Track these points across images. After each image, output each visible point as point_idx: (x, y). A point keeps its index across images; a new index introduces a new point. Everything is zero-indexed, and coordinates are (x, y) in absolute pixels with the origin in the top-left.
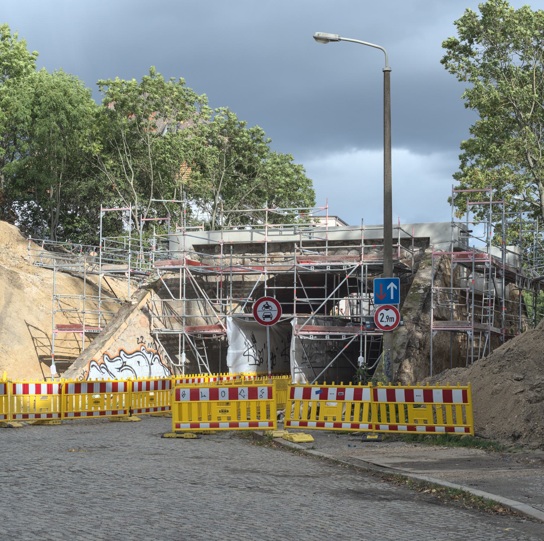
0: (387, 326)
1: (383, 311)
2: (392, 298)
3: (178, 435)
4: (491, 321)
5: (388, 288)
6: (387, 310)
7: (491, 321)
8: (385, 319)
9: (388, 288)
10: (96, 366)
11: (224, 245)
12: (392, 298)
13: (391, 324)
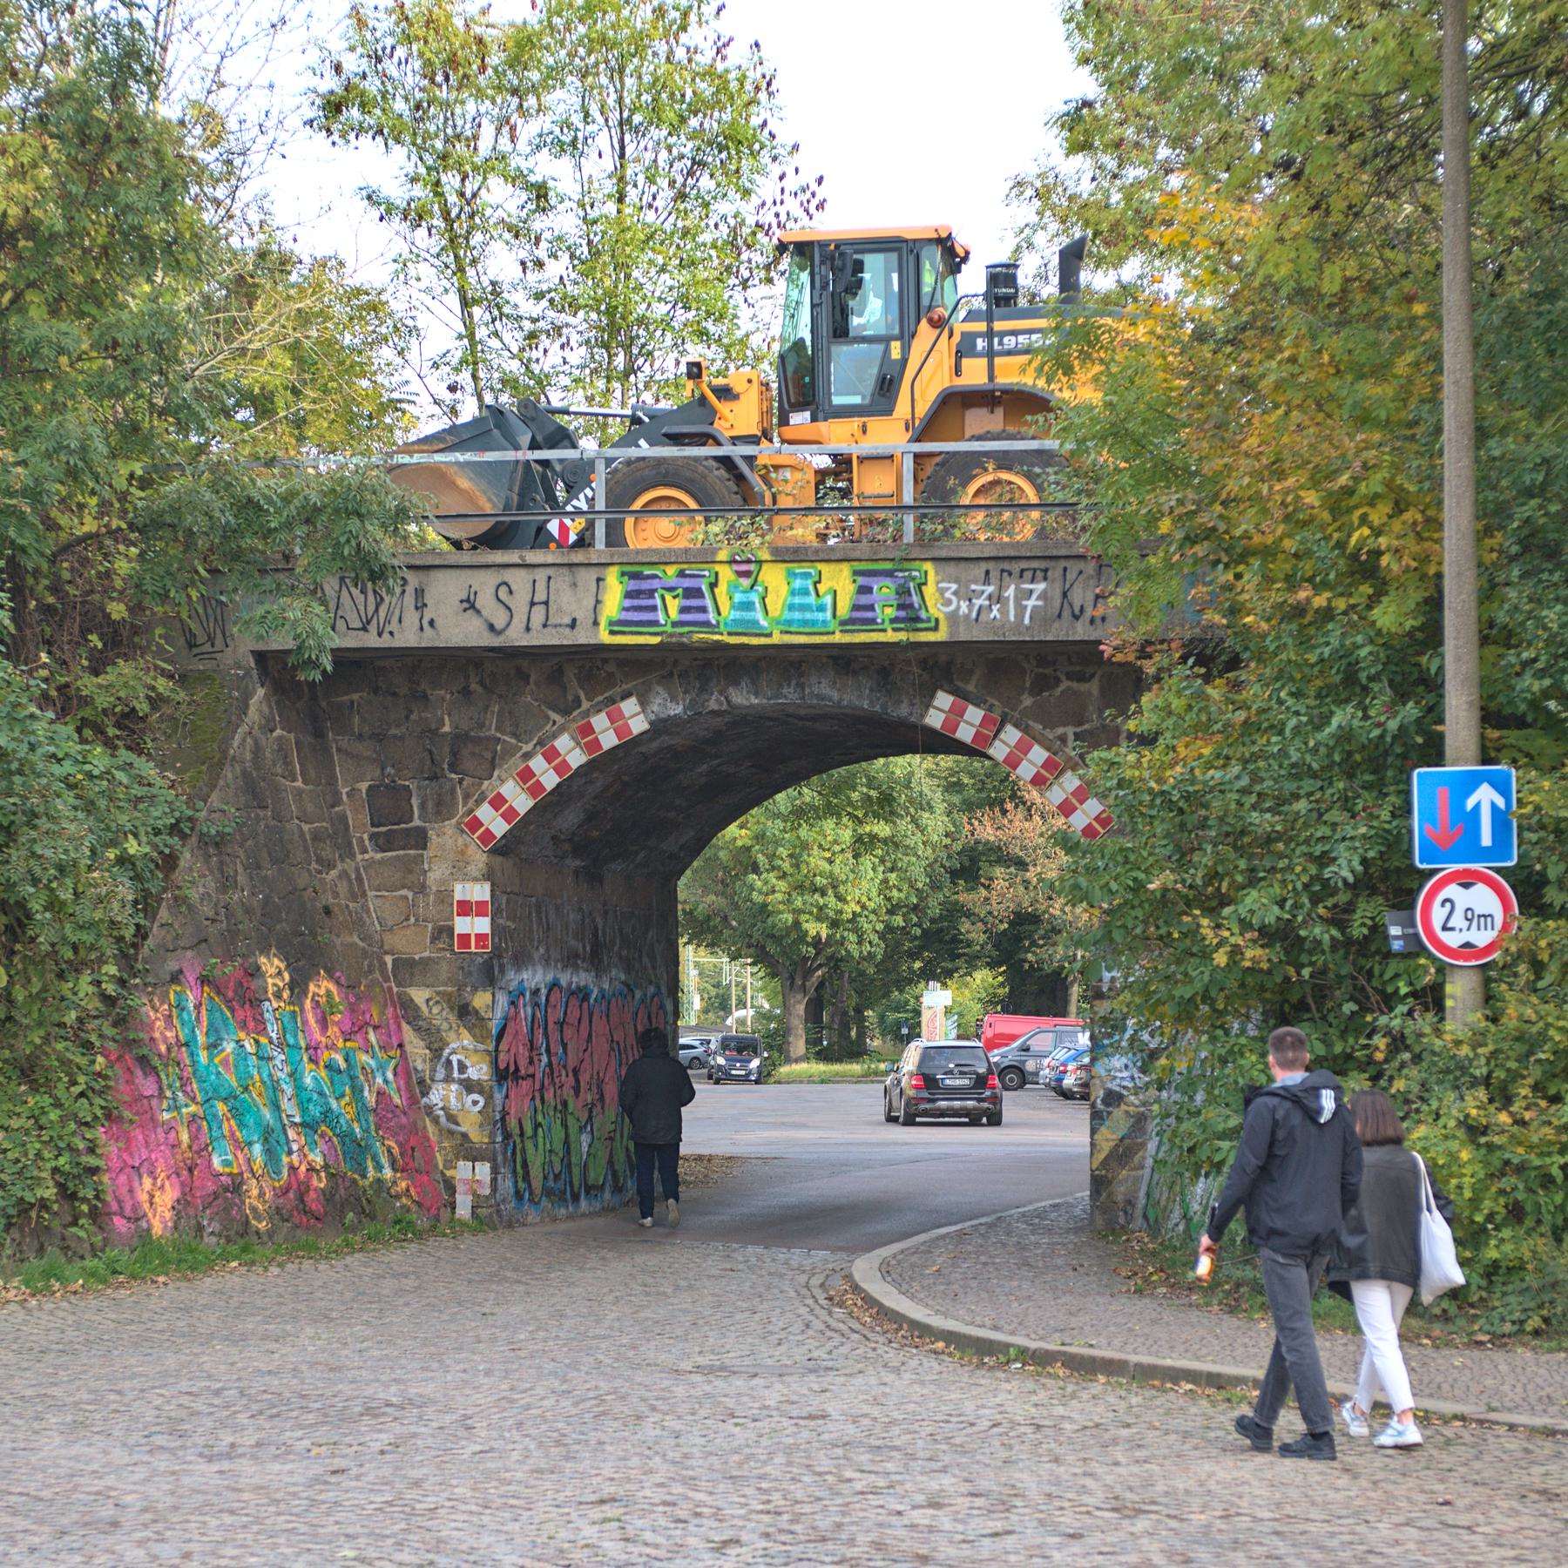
0: (1467, 945)
1: (1452, 891)
2: (1486, 840)
3: (636, 602)
4: (791, 608)
5: (1470, 803)
6: (1466, 886)
7: (791, 608)
8: (1458, 920)
9: (1470, 803)
10: (753, 440)
11: (1063, 1013)
12: (1486, 840)
13: (1482, 938)
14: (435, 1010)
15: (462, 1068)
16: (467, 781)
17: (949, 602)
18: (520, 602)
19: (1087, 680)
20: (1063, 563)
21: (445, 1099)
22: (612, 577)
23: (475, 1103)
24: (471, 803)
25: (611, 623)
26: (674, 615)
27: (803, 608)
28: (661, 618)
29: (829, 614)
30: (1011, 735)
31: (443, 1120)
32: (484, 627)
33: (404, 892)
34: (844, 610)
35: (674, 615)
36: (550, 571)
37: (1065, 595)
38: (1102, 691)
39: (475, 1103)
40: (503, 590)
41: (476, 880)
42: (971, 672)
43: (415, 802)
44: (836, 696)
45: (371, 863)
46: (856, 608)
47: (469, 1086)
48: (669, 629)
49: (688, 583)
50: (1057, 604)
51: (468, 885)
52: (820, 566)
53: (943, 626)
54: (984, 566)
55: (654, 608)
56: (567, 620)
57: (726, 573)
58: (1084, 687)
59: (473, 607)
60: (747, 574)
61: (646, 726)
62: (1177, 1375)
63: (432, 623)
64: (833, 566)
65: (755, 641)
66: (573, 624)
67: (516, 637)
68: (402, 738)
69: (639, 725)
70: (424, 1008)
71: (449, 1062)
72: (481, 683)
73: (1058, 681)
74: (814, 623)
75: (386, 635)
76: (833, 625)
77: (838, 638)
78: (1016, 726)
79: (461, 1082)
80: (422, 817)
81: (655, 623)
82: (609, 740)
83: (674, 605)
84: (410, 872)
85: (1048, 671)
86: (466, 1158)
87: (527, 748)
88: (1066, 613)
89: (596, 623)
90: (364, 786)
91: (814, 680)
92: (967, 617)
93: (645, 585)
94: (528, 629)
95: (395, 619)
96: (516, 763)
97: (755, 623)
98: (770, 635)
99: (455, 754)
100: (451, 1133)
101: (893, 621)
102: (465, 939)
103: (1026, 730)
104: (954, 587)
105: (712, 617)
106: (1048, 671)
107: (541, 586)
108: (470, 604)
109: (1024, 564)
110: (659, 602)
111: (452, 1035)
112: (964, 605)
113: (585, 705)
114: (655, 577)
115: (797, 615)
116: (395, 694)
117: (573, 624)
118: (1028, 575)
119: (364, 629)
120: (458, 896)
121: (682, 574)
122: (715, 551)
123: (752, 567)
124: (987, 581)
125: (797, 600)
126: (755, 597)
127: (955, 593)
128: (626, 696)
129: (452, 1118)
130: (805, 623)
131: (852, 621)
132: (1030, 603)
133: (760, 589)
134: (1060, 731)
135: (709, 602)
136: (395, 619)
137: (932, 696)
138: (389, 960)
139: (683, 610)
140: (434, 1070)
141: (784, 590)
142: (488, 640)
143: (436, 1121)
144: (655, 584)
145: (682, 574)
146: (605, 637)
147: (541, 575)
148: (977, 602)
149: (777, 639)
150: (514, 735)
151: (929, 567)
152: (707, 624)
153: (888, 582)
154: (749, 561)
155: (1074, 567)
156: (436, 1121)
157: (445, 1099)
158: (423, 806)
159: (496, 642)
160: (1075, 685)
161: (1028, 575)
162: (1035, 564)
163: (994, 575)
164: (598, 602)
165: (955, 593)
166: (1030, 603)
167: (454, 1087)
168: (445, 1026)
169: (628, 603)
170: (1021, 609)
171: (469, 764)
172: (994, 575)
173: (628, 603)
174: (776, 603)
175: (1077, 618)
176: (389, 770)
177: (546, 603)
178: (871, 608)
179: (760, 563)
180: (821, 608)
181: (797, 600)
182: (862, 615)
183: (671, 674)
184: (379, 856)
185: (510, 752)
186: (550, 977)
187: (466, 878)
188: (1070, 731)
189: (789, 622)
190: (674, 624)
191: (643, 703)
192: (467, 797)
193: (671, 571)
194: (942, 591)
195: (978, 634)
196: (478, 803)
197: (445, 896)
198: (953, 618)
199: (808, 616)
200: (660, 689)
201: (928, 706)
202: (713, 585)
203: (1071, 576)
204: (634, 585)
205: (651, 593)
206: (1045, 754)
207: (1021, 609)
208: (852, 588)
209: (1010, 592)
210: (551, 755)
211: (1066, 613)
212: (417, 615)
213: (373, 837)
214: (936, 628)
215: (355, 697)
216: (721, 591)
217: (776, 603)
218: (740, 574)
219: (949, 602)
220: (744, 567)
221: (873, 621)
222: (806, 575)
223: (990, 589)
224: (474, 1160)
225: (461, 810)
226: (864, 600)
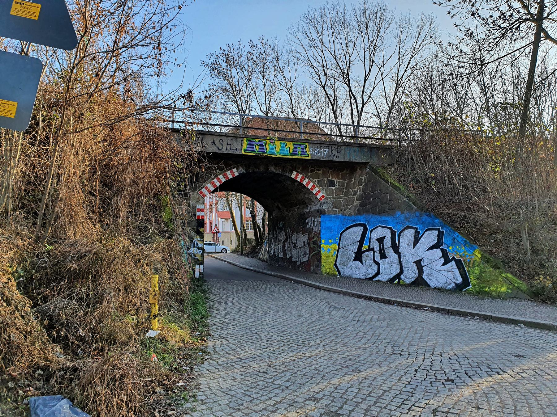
3: (250, 146)
4: (281, 150)
15: (197, 244)
18: (225, 144)
21: (193, 251)
22: (245, 140)
23: (200, 252)
24: (200, 188)
25: (245, 150)
27: (283, 150)
30: (307, 180)
31: (193, 256)
34: (291, 152)
35: (258, 149)
36: (231, 138)
38: (323, 173)
39: (200, 252)
44: (275, 171)
46: (293, 151)
48: (256, 152)
49: (260, 143)
51: (199, 205)
53: (310, 156)
54: (317, 145)
55: (254, 148)
56: (235, 149)
57: (268, 142)
58: (319, 172)
59: (214, 144)
60: (272, 142)
61: (238, 174)
62: (472, 315)
65: (274, 156)
66: (236, 150)
67: (224, 151)
69: (236, 174)
71: (194, 243)
73: (315, 171)
74: (285, 153)
76: (289, 154)
77: (290, 157)
79: (197, 247)
81: (254, 151)
82: (230, 177)
83: (257, 148)
88: (332, 155)
89: (241, 150)
92: (314, 155)
93: (252, 143)
94: (227, 150)
97: (274, 152)
100: (194, 258)
101: (301, 154)
102: (199, 217)
103: (309, 179)
105: (265, 150)
107: (229, 141)
108: (214, 143)
111: (195, 237)
112: (314, 152)
113: (225, 169)
115: (282, 152)
117: (236, 150)
118: (325, 147)
121: (259, 141)
122: (267, 137)
123: (273, 141)
124: (318, 148)
125: (282, 149)
128: (234, 168)
129: (195, 256)
130: (284, 153)
131: (292, 154)
132: (326, 153)
134: (315, 180)
137: (293, 172)
140: (191, 245)
141: (280, 146)
145: (259, 141)
147: (230, 138)
149: (278, 156)
151: (307, 144)
152: (264, 152)
153: (299, 146)
154: (273, 140)
155: (333, 147)
157: (193, 251)
159: (220, 152)
161: (325, 147)
162: (326, 145)
163: (319, 147)
164: (242, 145)
166: (326, 153)
167: (195, 248)
168: (193, 235)
169: (248, 146)
170: (324, 154)
172: (319, 147)
174: (278, 149)
177: (231, 144)
179: (275, 140)
181: (282, 149)
188: (317, 180)
189: (281, 153)
190: (258, 151)
191: (237, 169)
192: (199, 187)
193: (257, 140)
194: (309, 149)
195: (316, 158)
196: (202, 188)
197: (194, 208)
198: (311, 154)
199: (284, 152)
201: (292, 174)
202: (266, 144)
203: (333, 148)
204: (249, 142)
205: (253, 145)
207: (324, 154)
210: (218, 179)
211: (332, 155)
214: (308, 156)
216: (267, 145)
217: (278, 149)
218: (271, 142)
219: (311, 152)
220: (272, 141)
221: (297, 154)
222: (284, 144)
223: (318, 149)
224: (199, 264)
226: (295, 150)
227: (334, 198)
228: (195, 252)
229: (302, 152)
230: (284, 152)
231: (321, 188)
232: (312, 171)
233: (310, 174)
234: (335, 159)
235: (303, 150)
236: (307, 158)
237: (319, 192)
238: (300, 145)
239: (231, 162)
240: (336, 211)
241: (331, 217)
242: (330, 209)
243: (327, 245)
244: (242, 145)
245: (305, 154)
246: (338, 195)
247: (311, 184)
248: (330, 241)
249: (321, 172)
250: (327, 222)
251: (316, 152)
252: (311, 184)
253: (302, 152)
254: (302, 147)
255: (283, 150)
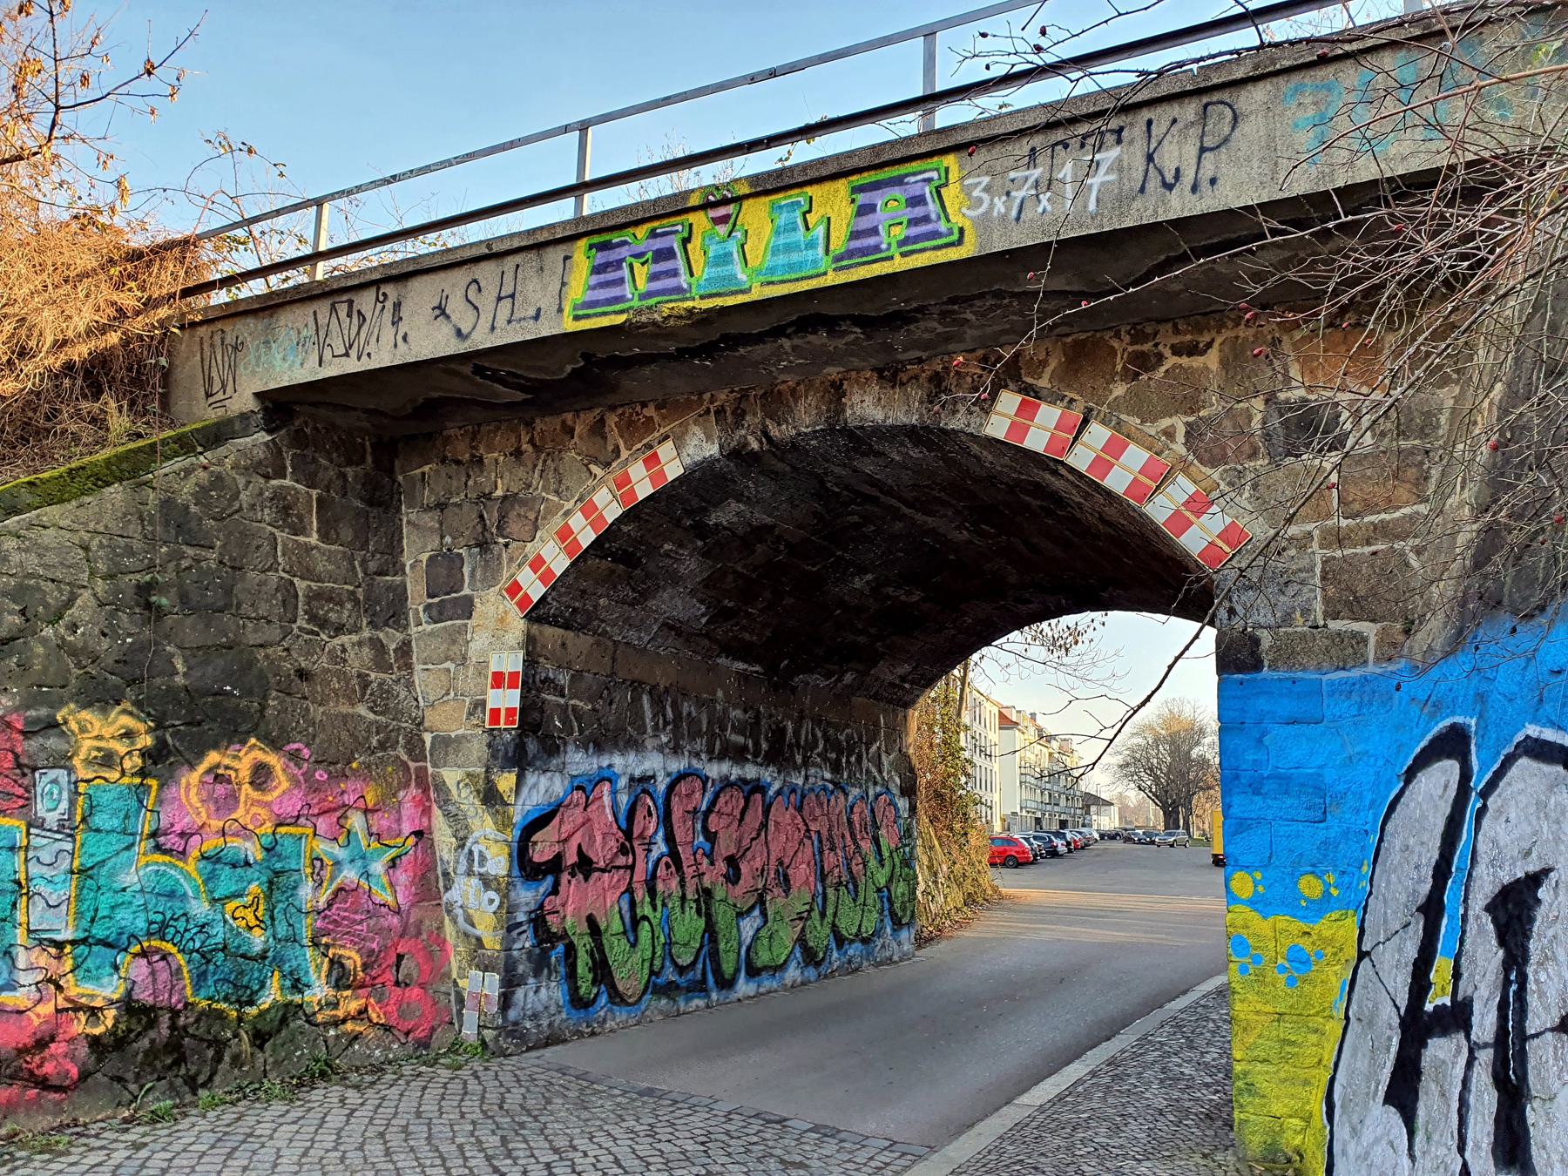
3: (603, 277)
7: (775, 251)
14: (464, 793)
16: (513, 545)
17: (980, 201)
19: (1202, 353)
20: (1146, 114)
26: (642, 285)
27: (789, 248)
28: (628, 290)
29: (821, 250)
30: (1098, 434)
31: (461, 919)
32: (453, 332)
33: (448, 664)
34: (839, 243)
35: (642, 285)
36: (518, 259)
37: (1150, 158)
38: (1224, 363)
39: (491, 901)
40: (474, 287)
41: (512, 648)
42: (1043, 364)
43: (466, 570)
45: (422, 635)
46: (855, 235)
47: (486, 881)
48: (636, 303)
49: (659, 244)
50: (1138, 175)
52: (809, 190)
53: (969, 237)
56: (532, 312)
58: (1197, 362)
59: (443, 313)
60: (723, 220)
63: (405, 338)
64: (828, 187)
65: (730, 301)
67: (482, 340)
68: (459, 506)
69: (673, 471)
70: (454, 791)
71: (471, 852)
72: (531, 441)
73: (1160, 358)
74: (801, 265)
75: (364, 357)
76: (826, 263)
77: (832, 279)
78: (1103, 422)
80: (472, 585)
84: (454, 642)
85: (1147, 347)
86: (478, 967)
87: (568, 505)
88: (1154, 183)
89: (560, 310)
90: (425, 557)
91: (856, 398)
92: (1003, 218)
93: (613, 255)
95: (374, 339)
96: (557, 522)
97: (733, 277)
98: (748, 291)
99: (503, 518)
100: (466, 935)
103: (1118, 428)
104: (986, 180)
105: (683, 280)
106: (1147, 347)
107: (509, 277)
109: (1083, 129)
110: (626, 272)
113: (625, 454)
114: (625, 243)
115: (782, 259)
116: (458, 462)
119: (347, 355)
120: (493, 668)
121: (653, 234)
125: (782, 240)
126: (733, 247)
127: (987, 189)
130: (791, 267)
131: (850, 254)
133: (738, 234)
134: (1165, 423)
135: (680, 262)
136: (374, 339)
138: (428, 737)
139: (654, 277)
141: (768, 228)
142: (454, 347)
143: (454, 921)
144: (624, 252)
145: (653, 234)
146: (570, 326)
148: (1018, 195)
149: (757, 294)
150: (557, 492)
152: (679, 290)
153: (896, 192)
156: (454, 921)
157: (465, 894)
158: (472, 575)
160: (1184, 361)
165: (987, 189)
168: (471, 812)
169: (595, 279)
171: (514, 527)
173: (595, 279)
174: (757, 251)
175: (1169, 187)
176: (448, 539)
178: (874, 231)
180: (811, 245)
182: (863, 243)
183: (708, 411)
184: (429, 628)
185: (551, 512)
186: (677, 765)
187: (503, 647)
188: (1179, 423)
189: (772, 270)
190: (643, 297)
192: (511, 560)
193: (642, 231)
194: (967, 191)
199: (795, 257)
200: (696, 429)
202: (686, 241)
204: (602, 258)
206: (1145, 455)
208: (850, 210)
209: (1067, 171)
211: (1154, 183)
212: (393, 331)
213: (428, 608)
214: (960, 242)
215: (426, 468)
218: (717, 221)
223: (1036, 173)
224: (485, 969)
225: (505, 575)
226: (865, 222)
227: (1338, 538)
228: (472, 901)
229: (913, 222)
230: (795, 257)
231: (1216, 474)
232: (1144, 362)
233: (1119, 390)
234: (1180, 205)
235: (919, 211)
236: (954, 254)
237: (1198, 504)
238: (899, 181)
239: (650, 411)
240: (1362, 640)
241: (1316, 691)
242: (1300, 626)
243: (1282, 921)
244: (563, 284)
245: (936, 234)
246: (1370, 508)
247: (1135, 456)
248: (1310, 887)
249: (1212, 359)
250: (1277, 733)
251: (1018, 195)
252: (1135, 456)
253: (913, 222)
254: (915, 190)
255: (789, 248)
